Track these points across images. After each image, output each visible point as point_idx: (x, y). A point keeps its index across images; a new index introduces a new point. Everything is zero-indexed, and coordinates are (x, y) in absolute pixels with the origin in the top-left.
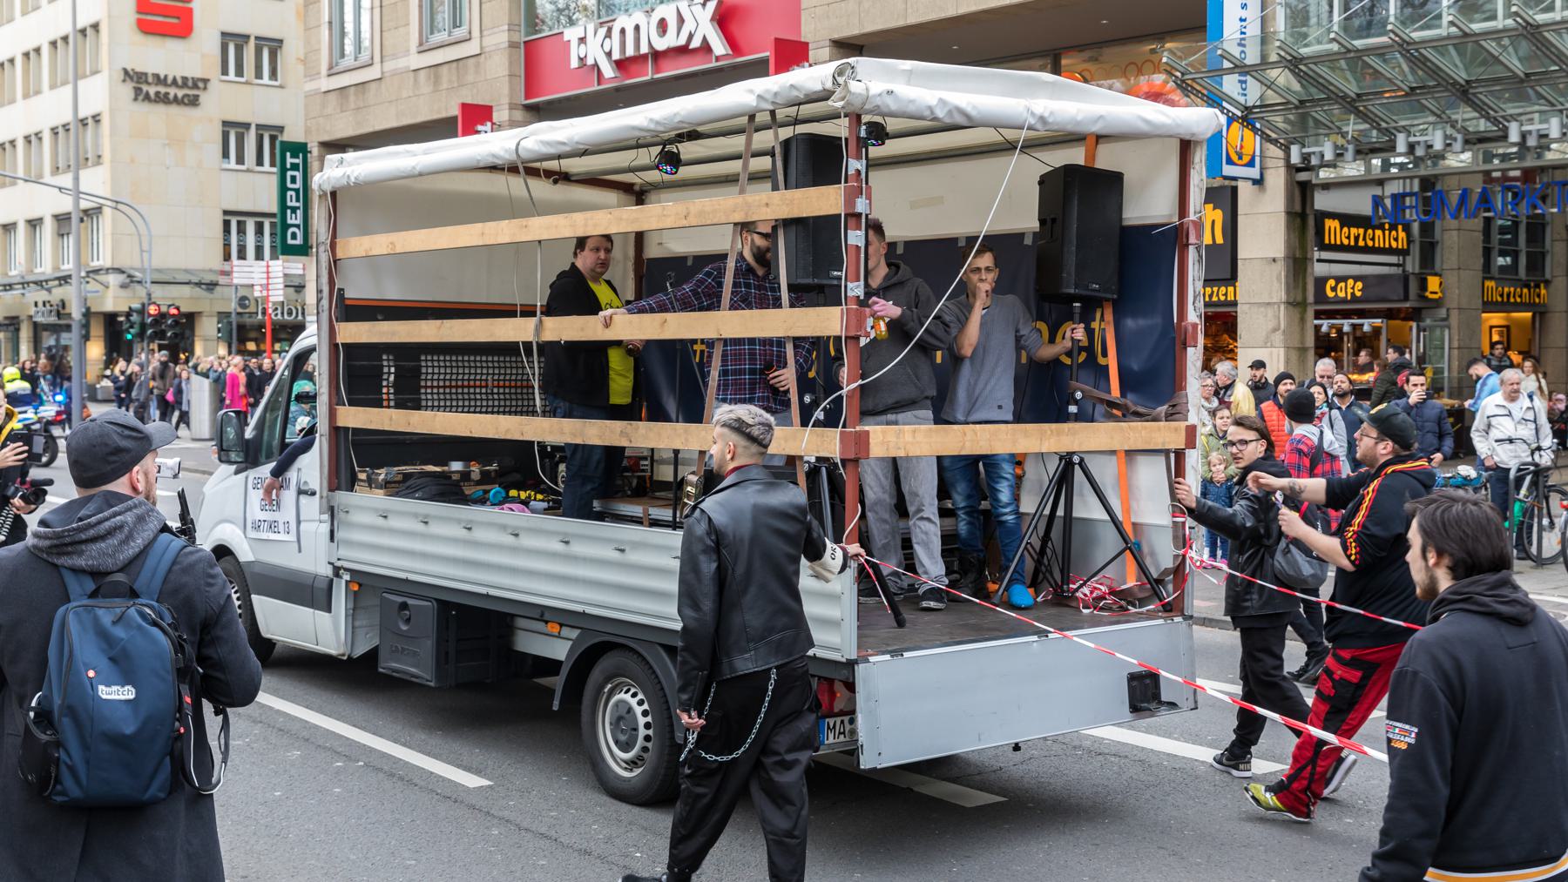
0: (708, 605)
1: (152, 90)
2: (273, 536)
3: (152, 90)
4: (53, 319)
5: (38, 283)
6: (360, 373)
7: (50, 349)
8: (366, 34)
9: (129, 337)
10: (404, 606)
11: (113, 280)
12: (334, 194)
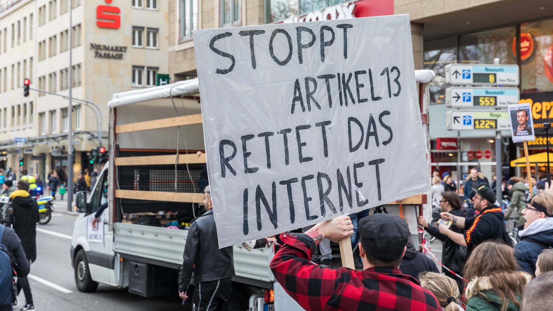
0: (192, 255)
1: (103, 53)
2: (96, 241)
3: (103, 53)
4: (59, 154)
5: (54, 139)
6: (125, 177)
7: (58, 167)
8: (195, 25)
9: (92, 162)
10: (136, 266)
11: (85, 137)
12: (115, 109)
